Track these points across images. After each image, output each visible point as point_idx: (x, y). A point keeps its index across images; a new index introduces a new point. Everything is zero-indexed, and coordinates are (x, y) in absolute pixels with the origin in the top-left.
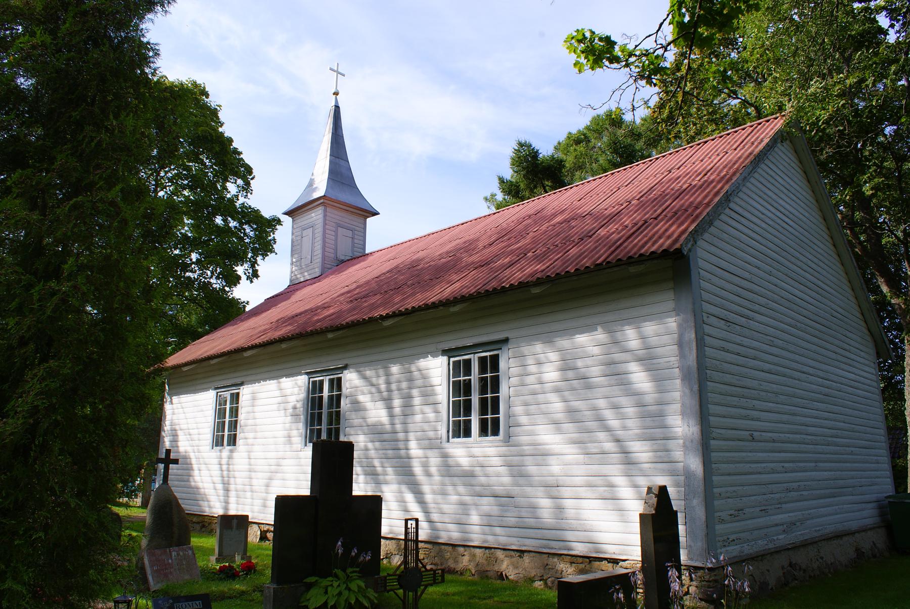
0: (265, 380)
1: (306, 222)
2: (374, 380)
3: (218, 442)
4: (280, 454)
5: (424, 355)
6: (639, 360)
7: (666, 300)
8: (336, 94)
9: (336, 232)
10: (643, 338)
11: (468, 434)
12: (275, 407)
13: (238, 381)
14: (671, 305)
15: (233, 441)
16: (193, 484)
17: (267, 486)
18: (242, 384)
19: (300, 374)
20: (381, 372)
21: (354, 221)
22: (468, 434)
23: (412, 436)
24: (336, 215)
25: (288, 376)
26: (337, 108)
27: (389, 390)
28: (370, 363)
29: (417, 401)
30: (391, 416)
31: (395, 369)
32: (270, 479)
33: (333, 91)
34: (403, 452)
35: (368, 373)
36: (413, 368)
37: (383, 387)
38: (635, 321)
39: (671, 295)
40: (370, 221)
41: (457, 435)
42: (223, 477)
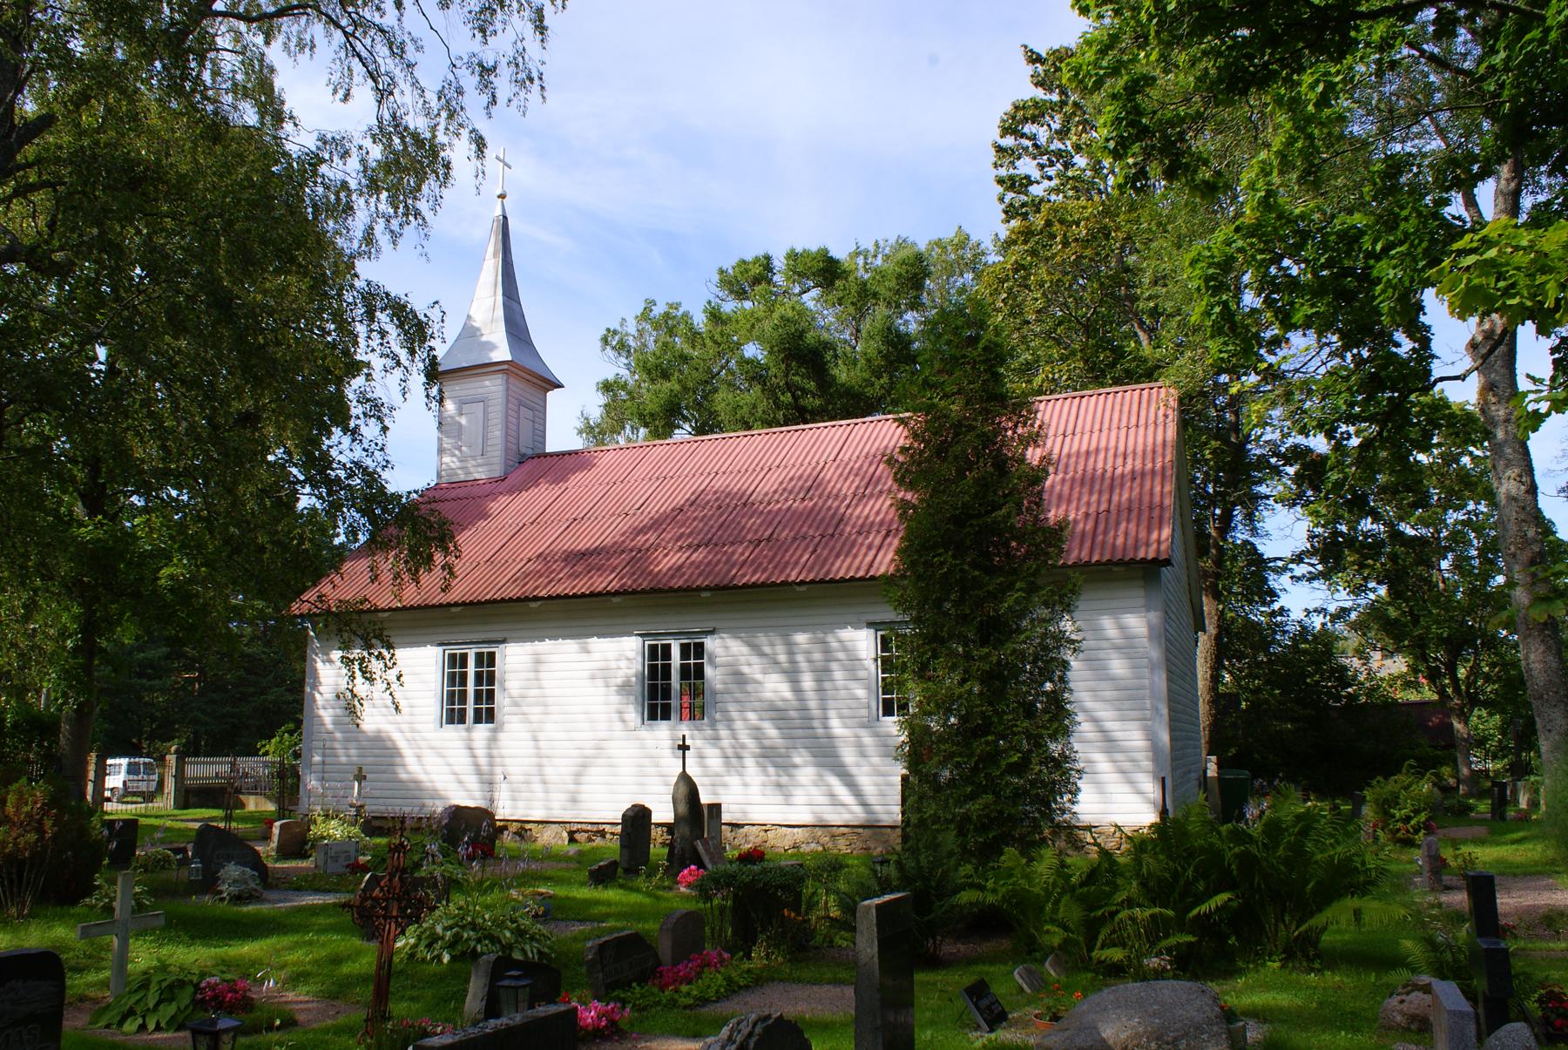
0: (564, 637)
1: (472, 392)
2: (767, 649)
3: (455, 716)
4: (601, 735)
5: (844, 625)
6: (1117, 648)
7: (1137, 595)
8: (502, 196)
9: (518, 412)
10: (1122, 628)
11: (462, 721)
12: (586, 674)
13: (499, 636)
14: (1141, 601)
15: (486, 715)
16: (403, 776)
17: (578, 775)
18: (504, 641)
19: (630, 634)
20: (778, 640)
21: (530, 393)
22: (462, 721)
23: (832, 713)
24: (518, 387)
25: (600, 635)
26: (505, 218)
27: (793, 662)
28: (764, 629)
29: (838, 675)
30: (797, 690)
31: (801, 638)
32: (584, 766)
33: (499, 192)
34: (820, 731)
35: (762, 639)
36: (830, 638)
37: (782, 658)
38: (1115, 612)
39: (1141, 592)
40: (552, 396)
41: (450, 721)
42: (477, 765)
